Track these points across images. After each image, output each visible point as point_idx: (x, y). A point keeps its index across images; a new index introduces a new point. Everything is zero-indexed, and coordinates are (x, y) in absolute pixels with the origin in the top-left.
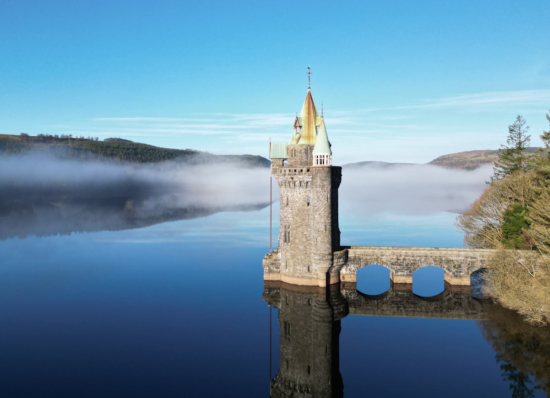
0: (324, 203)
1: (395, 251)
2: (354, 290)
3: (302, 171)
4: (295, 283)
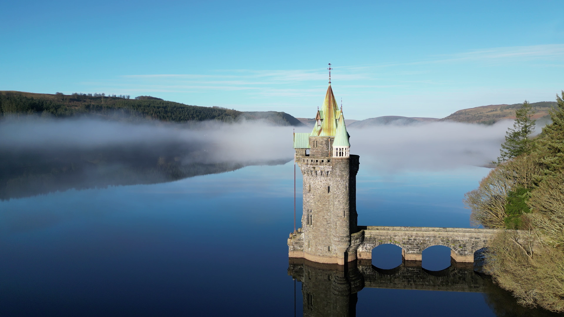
0: (343, 192)
1: (407, 232)
2: (369, 266)
3: (323, 161)
4: (317, 261)
